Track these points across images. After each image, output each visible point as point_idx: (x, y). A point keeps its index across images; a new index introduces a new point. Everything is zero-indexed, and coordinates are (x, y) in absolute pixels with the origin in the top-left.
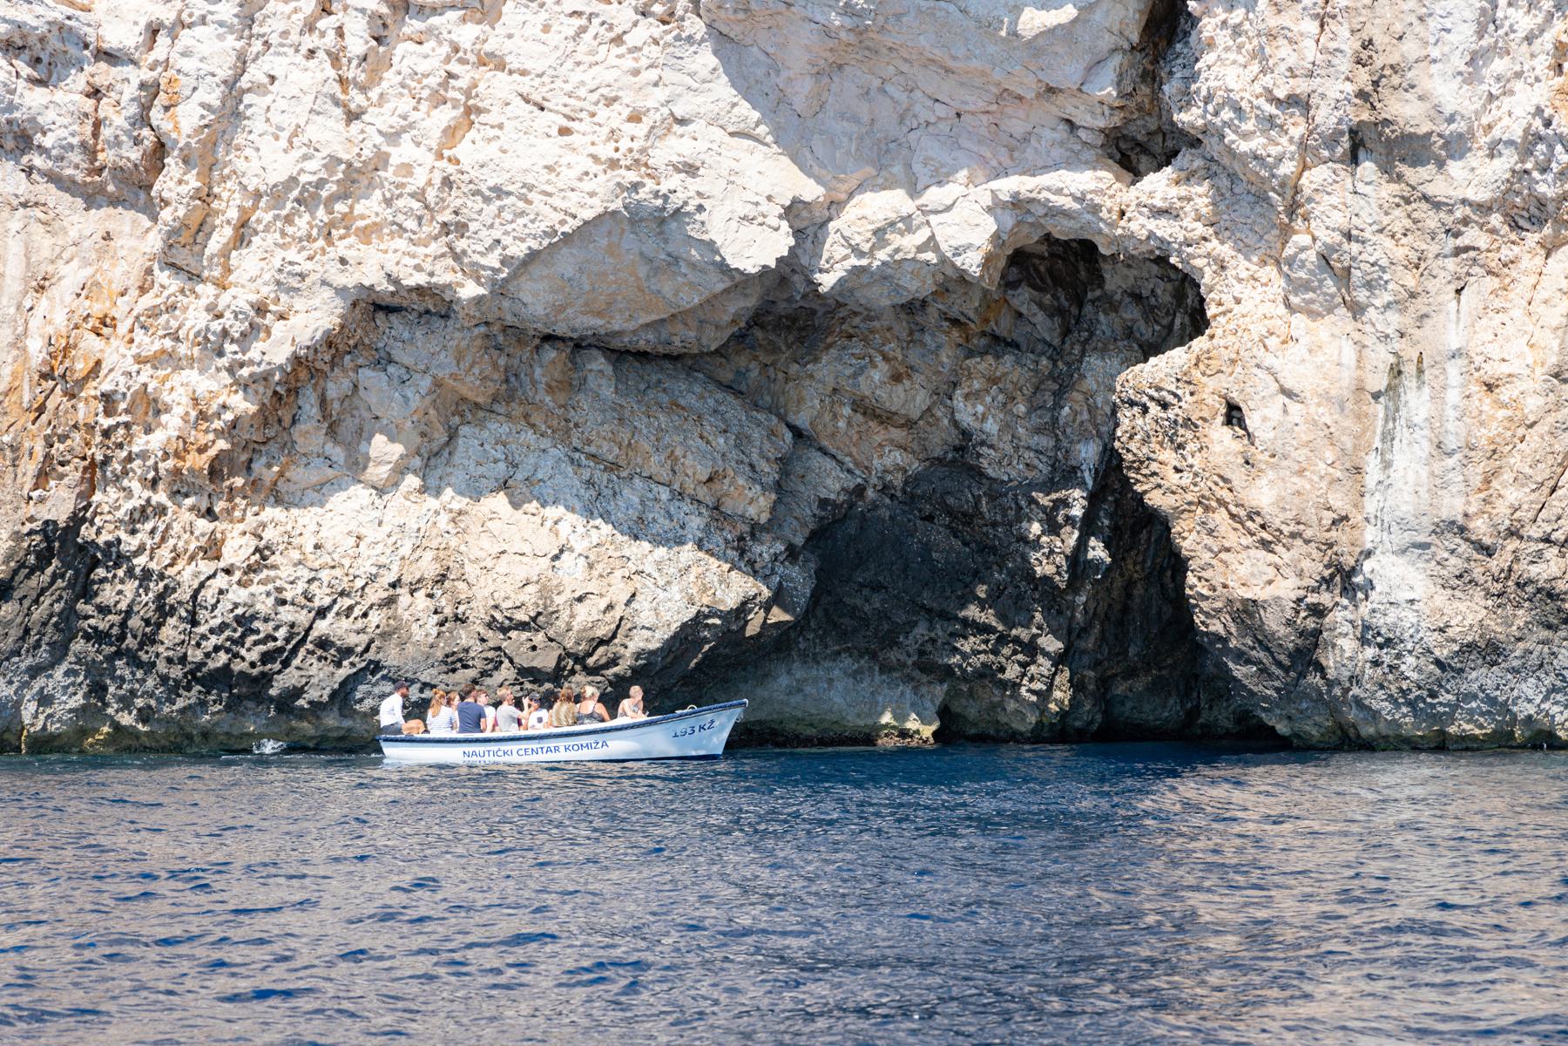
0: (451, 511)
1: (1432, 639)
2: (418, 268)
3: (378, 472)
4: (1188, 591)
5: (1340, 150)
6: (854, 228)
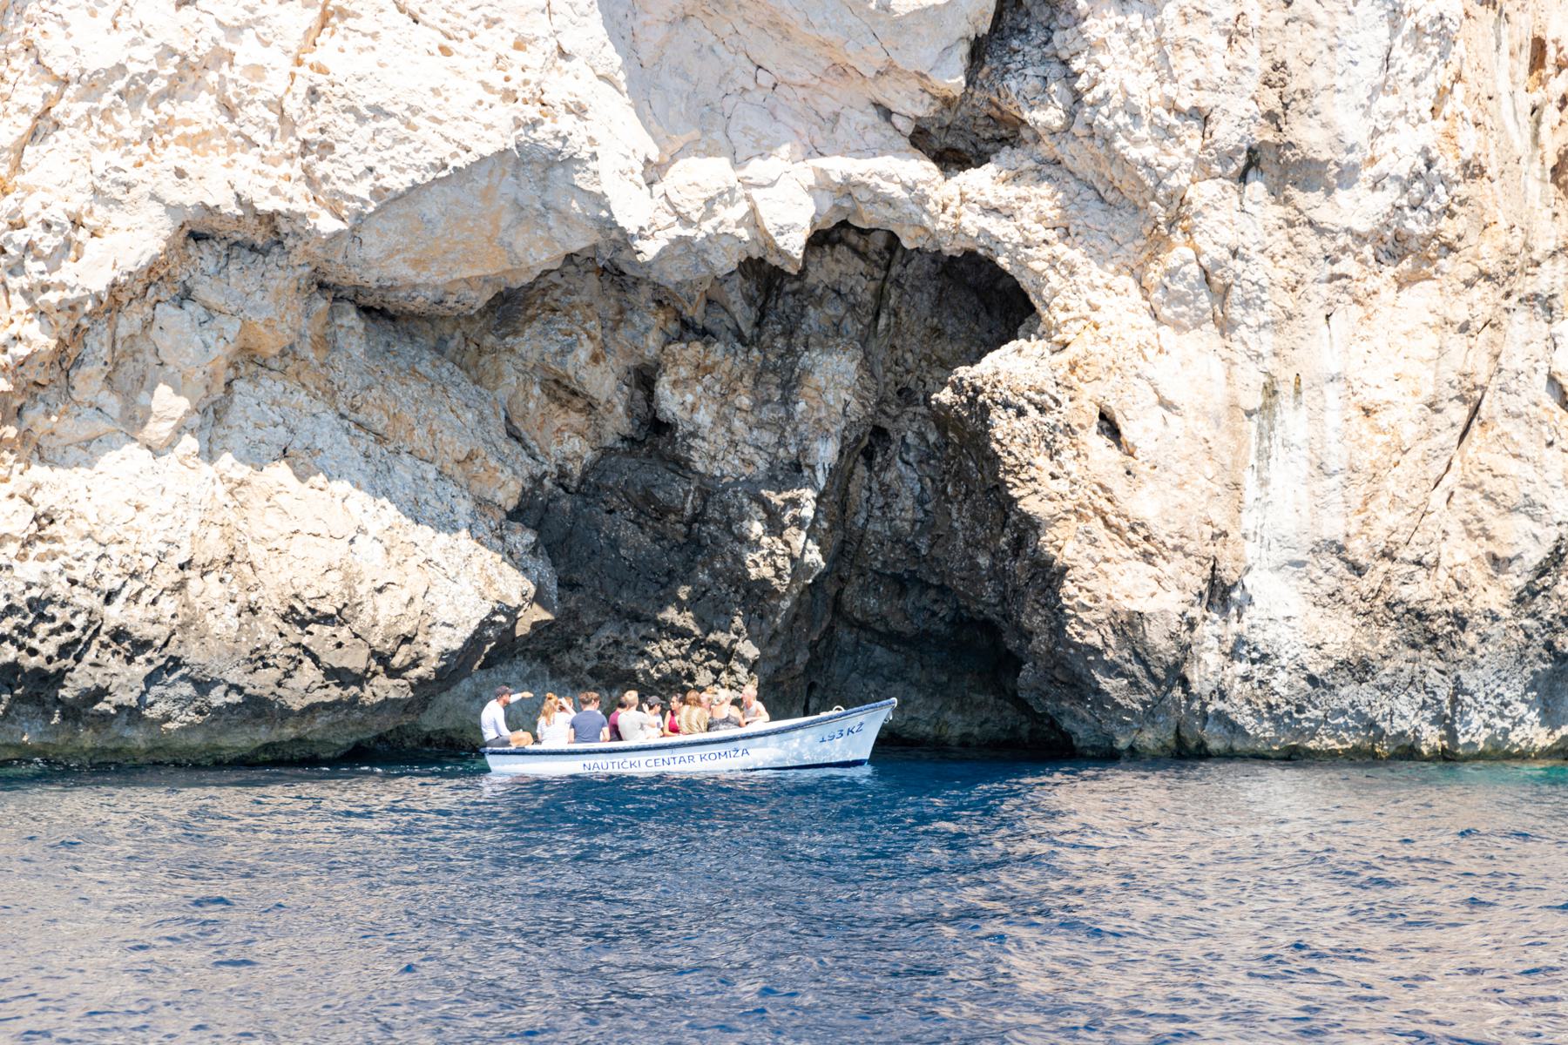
0: (230, 480)
1: (1308, 656)
2: (274, 191)
3: (158, 430)
4: (1065, 601)
5: (1233, 168)
6: (684, 195)
